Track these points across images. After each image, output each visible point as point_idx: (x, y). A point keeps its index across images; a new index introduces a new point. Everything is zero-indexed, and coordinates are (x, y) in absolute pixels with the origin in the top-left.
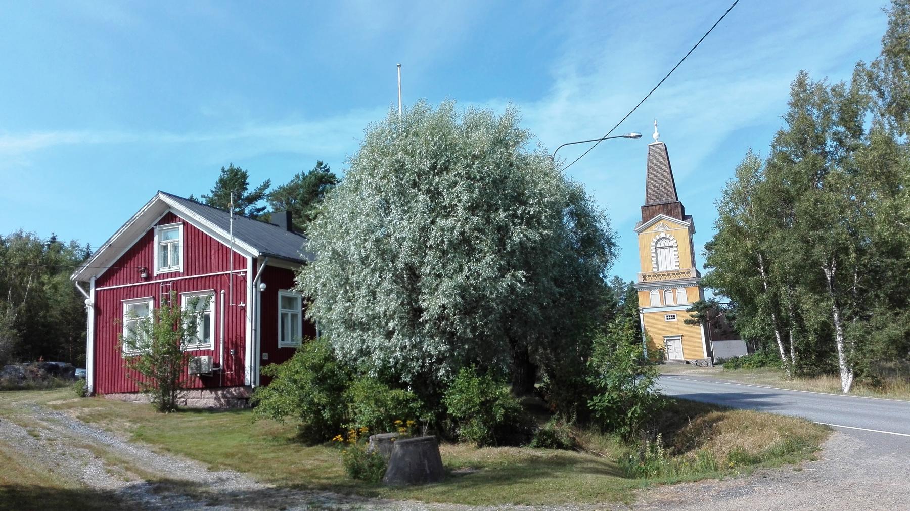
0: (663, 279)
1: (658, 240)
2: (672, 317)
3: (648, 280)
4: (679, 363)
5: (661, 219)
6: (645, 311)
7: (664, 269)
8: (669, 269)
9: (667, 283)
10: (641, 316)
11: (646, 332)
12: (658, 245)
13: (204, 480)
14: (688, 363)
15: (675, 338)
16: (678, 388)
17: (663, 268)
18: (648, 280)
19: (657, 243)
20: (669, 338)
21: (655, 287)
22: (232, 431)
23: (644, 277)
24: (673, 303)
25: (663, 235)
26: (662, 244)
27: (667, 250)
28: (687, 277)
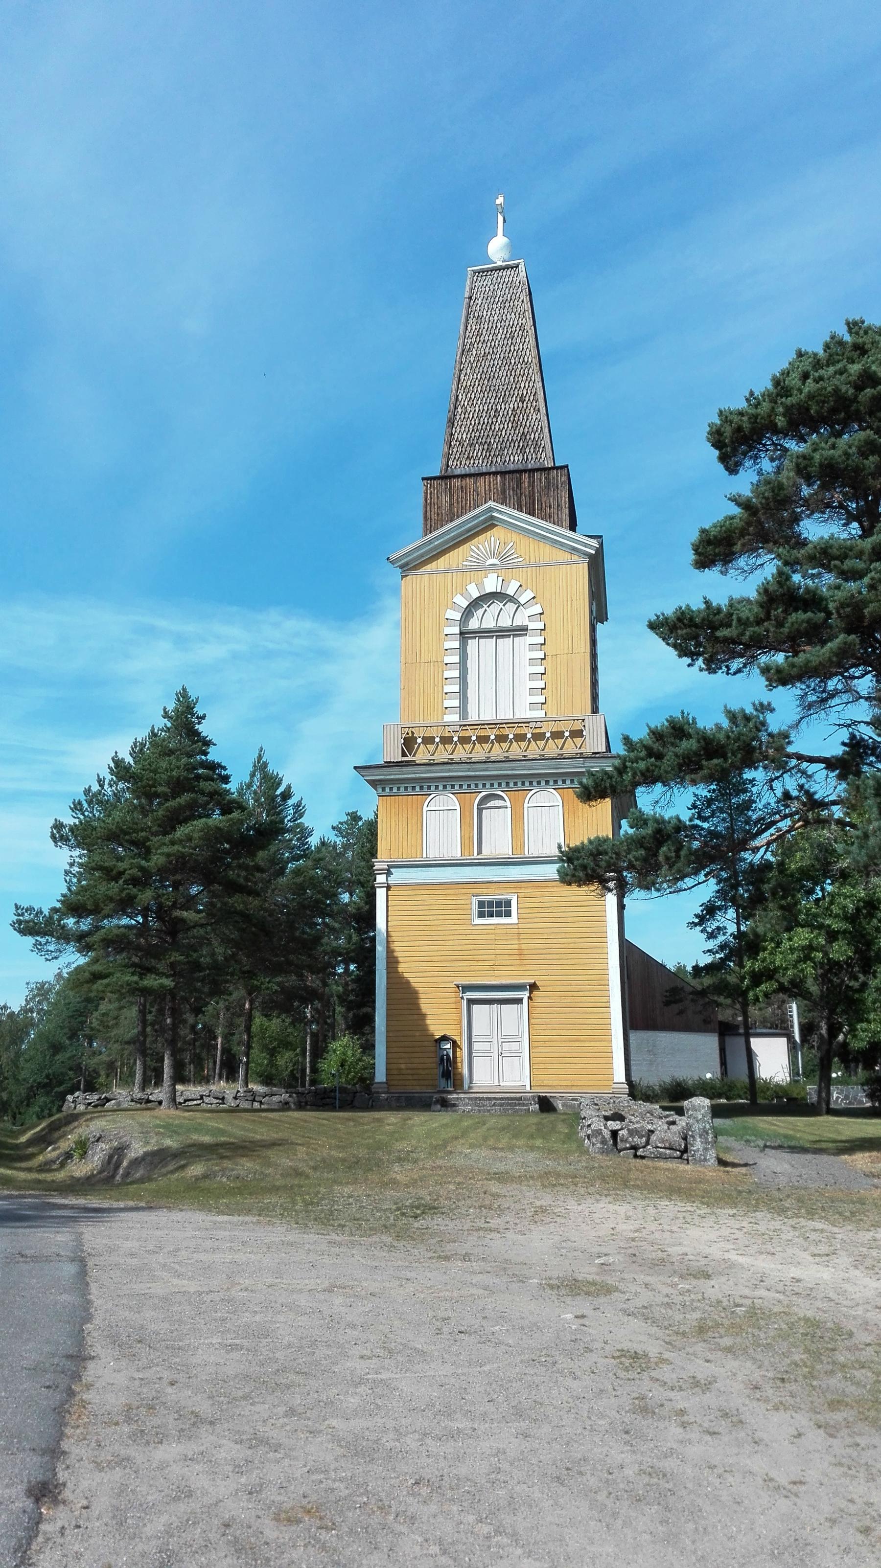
0: (479, 753)
1: (475, 604)
2: (501, 908)
3: (422, 755)
4: (510, 1103)
5: (489, 524)
6: (398, 875)
7: (488, 715)
8: (506, 715)
9: (487, 768)
10: (381, 894)
11: (392, 961)
12: (473, 624)
13: (28, 1497)
14: (546, 1105)
15: (501, 994)
16: (831, 1136)
17: (482, 710)
18: (422, 755)
19: (468, 612)
20: (478, 994)
21: (447, 783)
22: (362, 1069)
23: (409, 743)
24: (455, 852)
25: (491, 584)
26: (489, 617)
27: (505, 643)
28: (571, 748)
